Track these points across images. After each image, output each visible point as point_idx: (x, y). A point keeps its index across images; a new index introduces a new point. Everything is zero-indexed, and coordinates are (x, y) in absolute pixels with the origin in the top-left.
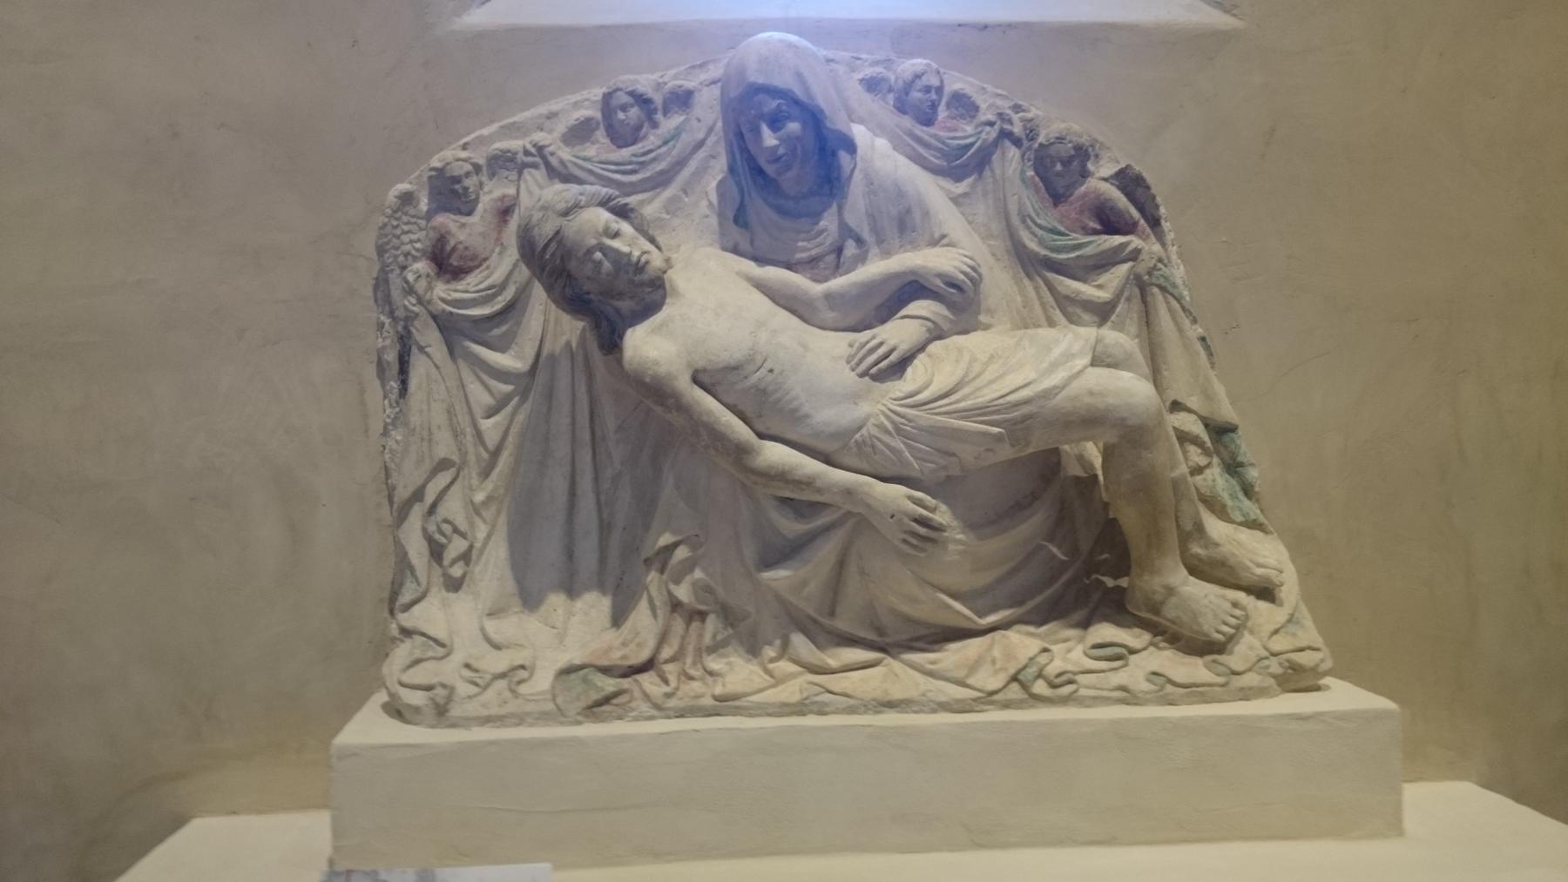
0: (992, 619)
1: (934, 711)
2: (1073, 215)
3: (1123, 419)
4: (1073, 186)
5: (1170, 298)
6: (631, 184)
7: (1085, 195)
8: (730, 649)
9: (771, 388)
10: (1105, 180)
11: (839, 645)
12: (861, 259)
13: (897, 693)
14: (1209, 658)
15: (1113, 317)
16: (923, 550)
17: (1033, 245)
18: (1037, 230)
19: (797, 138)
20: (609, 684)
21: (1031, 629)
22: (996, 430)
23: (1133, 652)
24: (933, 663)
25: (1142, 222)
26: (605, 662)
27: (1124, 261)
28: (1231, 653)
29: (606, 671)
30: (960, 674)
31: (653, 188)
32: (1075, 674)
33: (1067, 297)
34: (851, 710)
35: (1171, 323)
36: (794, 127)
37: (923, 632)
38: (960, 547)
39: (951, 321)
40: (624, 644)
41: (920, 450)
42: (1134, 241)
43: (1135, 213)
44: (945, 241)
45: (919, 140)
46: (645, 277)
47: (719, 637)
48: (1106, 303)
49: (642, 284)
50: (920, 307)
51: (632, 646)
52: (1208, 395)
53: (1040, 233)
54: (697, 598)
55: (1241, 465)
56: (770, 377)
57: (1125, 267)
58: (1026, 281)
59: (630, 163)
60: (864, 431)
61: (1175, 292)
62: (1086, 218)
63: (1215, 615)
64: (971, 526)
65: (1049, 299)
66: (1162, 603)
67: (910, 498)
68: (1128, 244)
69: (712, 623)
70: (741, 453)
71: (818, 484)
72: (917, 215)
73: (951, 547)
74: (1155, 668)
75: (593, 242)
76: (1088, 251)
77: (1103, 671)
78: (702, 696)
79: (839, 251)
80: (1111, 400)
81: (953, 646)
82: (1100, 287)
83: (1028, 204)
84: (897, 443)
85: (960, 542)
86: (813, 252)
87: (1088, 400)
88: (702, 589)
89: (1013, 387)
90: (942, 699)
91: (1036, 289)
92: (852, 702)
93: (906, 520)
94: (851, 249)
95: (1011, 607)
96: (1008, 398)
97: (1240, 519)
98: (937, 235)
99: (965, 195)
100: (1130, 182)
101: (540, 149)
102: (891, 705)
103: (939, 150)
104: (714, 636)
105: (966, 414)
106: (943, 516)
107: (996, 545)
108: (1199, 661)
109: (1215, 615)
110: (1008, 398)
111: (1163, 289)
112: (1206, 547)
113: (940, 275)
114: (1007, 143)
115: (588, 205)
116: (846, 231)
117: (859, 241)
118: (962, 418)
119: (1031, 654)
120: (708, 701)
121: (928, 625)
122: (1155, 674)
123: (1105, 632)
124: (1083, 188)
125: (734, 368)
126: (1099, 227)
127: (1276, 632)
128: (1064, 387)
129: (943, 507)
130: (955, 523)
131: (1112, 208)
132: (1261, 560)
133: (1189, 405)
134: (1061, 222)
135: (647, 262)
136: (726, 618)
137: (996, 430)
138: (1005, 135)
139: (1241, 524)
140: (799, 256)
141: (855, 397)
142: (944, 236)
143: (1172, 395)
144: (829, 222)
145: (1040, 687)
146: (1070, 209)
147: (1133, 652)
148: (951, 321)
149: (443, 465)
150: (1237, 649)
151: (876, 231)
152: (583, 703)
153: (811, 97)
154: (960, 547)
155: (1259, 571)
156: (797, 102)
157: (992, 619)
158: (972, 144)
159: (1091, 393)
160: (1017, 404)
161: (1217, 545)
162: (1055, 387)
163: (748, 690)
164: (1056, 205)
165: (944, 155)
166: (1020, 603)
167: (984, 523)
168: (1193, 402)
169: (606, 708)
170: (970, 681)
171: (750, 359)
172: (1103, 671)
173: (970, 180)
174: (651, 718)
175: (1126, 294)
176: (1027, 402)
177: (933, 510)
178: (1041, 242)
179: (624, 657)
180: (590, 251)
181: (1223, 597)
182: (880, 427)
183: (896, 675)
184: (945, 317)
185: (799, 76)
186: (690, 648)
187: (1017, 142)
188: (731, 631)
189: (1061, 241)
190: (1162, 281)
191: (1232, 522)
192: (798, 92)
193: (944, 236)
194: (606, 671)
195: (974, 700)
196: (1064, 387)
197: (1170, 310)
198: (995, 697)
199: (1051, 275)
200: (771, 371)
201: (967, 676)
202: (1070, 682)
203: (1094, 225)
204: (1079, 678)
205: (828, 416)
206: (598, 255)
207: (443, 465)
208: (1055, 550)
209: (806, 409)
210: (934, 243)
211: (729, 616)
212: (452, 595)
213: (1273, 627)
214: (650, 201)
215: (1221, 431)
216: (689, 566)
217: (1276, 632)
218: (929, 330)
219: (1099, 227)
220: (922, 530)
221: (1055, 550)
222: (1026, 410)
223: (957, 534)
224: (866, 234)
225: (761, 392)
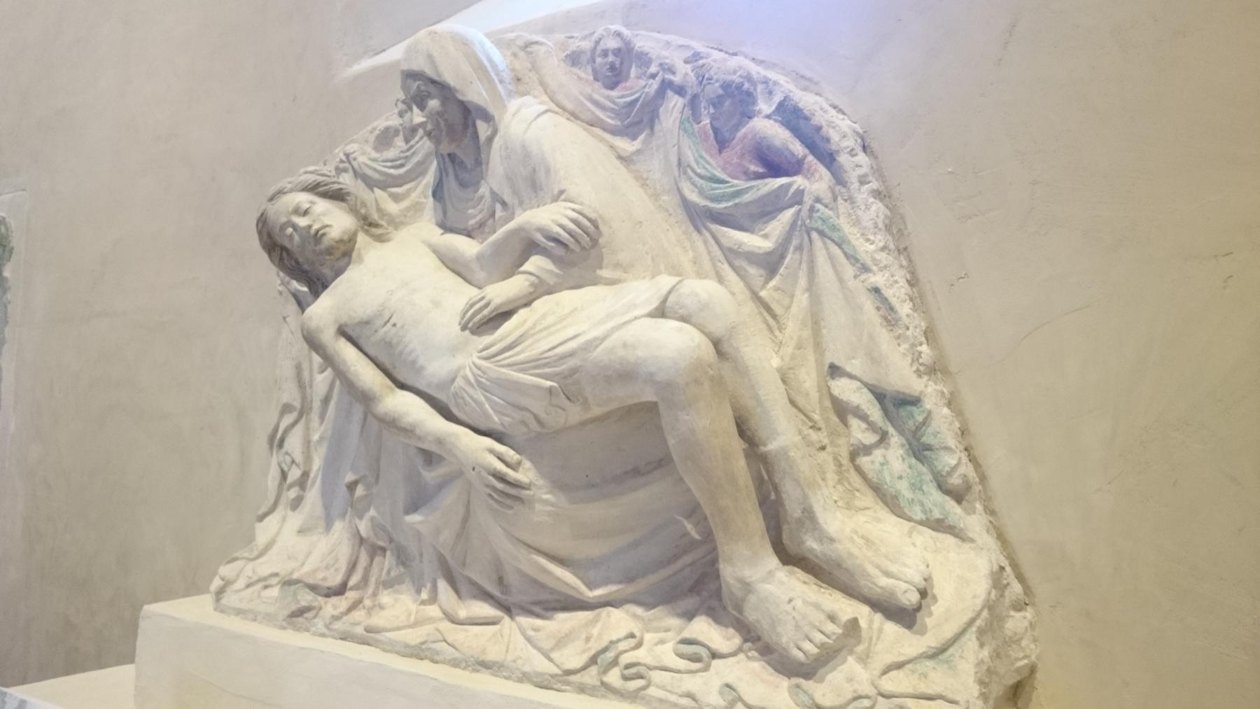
0: (599, 592)
1: (520, 681)
2: (735, 160)
3: (652, 374)
4: (737, 127)
5: (829, 242)
6: (400, 176)
7: (745, 136)
8: (403, 587)
9: (395, 341)
10: (768, 117)
11: (475, 597)
12: (511, 217)
13: (493, 655)
14: (795, 680)
15: (782, 270)
16: (511, 508)
17: (693, 197)
18: (697, 179)
19: (438, 113)
20: (306, 598)
21: (639, 611)
22: (549, 383)
23: (715, 655)
24: (536, 630)
25: (810, 158)
26: (311, 581)
27: (791, 206)
28: (821, 680)
29: (313, 588)
30: (546, 645)
31: (417, 178)
32: (650, 668)
33: (730, 250)
34: (455, 663)
35: (830, 272)
36: (434, 104)
37: (544, 596)
38: (549, 508)
39: (557, 276)
40: (327, 568)
41: (496, 403)
42: (799, 181)
43: (798, 148)
44: (563, 197)
45: (596, 103)
46: (322, 247)
47: (393, 574)
48: (769, 254)
49: (321, 253)
50: (536, 263)
51: (332, 570)
52: (874, 359)
53: (700, 182)
54: (376, 535)
55: (929, 448)
56: (394, 330)
57: (788, 215)
58: (695, 235)
59: (400, 158)
60: (456, 384)
61: (835, 236)
62: (753, 164)
63: (798, 627)
64: (560, 485)
65: (718, 253)
66: (743, 600)
67: (492, 451)
68: (790, 185)
69: (389, 560)
70: (366, 399)
71: (418, 432)
72: (541, 174)
73: (538, 507)
74: (730, 680)
75: (284, 219)
76: (747, 198)
77: (679, 672)
78: (358, 624)
79: (493, 215)
80: (640, 353)
81: (561, 616)
82: (766, 236)
83: (689, 153)
84: (479, 395)
85: (546, 502)
86: (478, 218)
87: (621, 353)
88: (376, 526)
89: (556, 343)
90: (527, 669)
91: (705, 242)
92: (457, 655)
93: (484, 474)
94: (499, 213)
95: (620, 582)
96: (557, 351)
97: (919, 516)
98: (556, 192)
99: (638, 152)
100: (791, 115)
101: (347, 155)
102: (485, 665)
103: (612, 110)
104: (389, 572)
105: (522, 366)
106: (526, 474)
107: (595, 511)
108: (785, 683)
109: (798, 627)
110: (557, 351)
111: (822, 233)
112: (821, 541)
113: (541, 230)
114: (670, 93)
115: (291, 191)
116: (496, 198)
117: (504, 204)
118: (523, 371)
119: (614, 638)
120: (360, 630)
121: (552, 591)
122: (728, 686)
123: (703, 629)
124: (744, 130)
125: (367, 323)
126: (761, 170)
127: (899, 666)
128: (603, 339)
129: (527, 464)
130: (541, 482)
131: (769, 148)
132: (894, 568)
133: (848, 369)
134: (724, 170)
135: (324, 235)
136: (398, 557)
137: (549, 383)
138: (666, 86)
139: (921, 523)
140: (472, 222)
141: (454, 350)
142: (562, 192)
143: (830, 358)
144: (484, 190)
145: (613, 677)
146: (731, 154)
147: (715, 655)
148: (557, 276)
149: (286, 409)
150: (829, 677)
151: (516, 192)
152: (287, 612)
153: (438, 74)
154: (549, 508)
155: (884, 581)
156: (433, 82)
157: (599, 592)
158: (637, 100)
159: (625, 345)
160: (563, 357)
161: (832, 540)
162: (596, 339)
163: (388, 626)
164: (720, 152)
165: (617, 114)
166: (630, 580)
167: (577, 482)
168: (853, 366)
169: (300, 619)
170: (554, 655)
171: (379, 314)
172: (679, 672)
173: (642, 137)
174: (323, 635)
175: (795, 242)
176: (571, 354)
177: (514, 467)
178: (701, 193)
179: (324, 579)
180: (283, 227)
181: (817, 606)
182: (466, 378)
183: (512, 638)
184: (551, 272)
185: (430, 57)
186: (373, 580)
187: (680, 91)
188: (402, 569)
189: (721, 190)
190: (819, 224)
191: (910, 519)
192: (429, 72)
193: (562, 192)
194: (313, 588)
195: (553, 676)
196: (603, 339)
197: (831, 258)
198: (573, 678)
199: (715, 227)
200: (394, 325)
201: (552, 649)
202: (642, 677)
203: (754, 168)
204: (657, 676)
205: (436, 368)
206: (290, 230)
207: (286, 409)
208: (689, 527)
209: (421, 361)
210: (556, 199)
211: (403, 558)
212: (290, 513)
213: (890, 659)
214: (415, 188)
215: (896, 404)
216: (368, 500)
217: (899, 666)
218: (532, 284)
219: (761, 170)
220: (500, 486)
221: (689, 527)
222: (571, 363)
223: (543, 495)
224: (507, 198)
225: (389, 345)
